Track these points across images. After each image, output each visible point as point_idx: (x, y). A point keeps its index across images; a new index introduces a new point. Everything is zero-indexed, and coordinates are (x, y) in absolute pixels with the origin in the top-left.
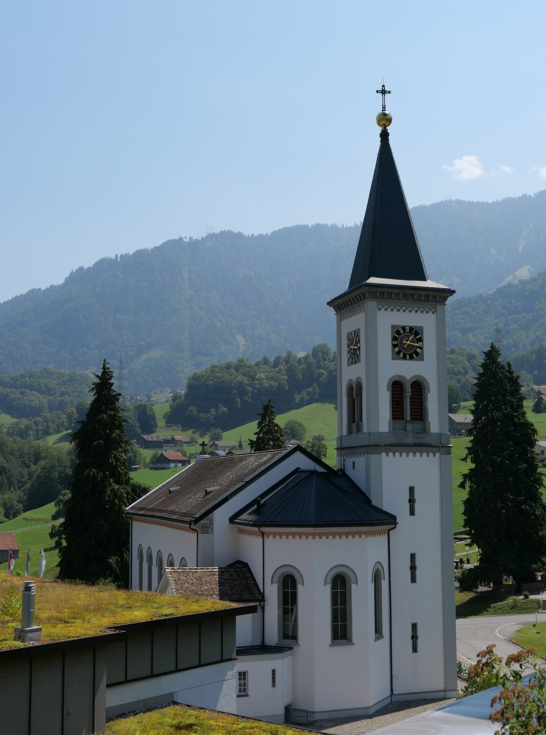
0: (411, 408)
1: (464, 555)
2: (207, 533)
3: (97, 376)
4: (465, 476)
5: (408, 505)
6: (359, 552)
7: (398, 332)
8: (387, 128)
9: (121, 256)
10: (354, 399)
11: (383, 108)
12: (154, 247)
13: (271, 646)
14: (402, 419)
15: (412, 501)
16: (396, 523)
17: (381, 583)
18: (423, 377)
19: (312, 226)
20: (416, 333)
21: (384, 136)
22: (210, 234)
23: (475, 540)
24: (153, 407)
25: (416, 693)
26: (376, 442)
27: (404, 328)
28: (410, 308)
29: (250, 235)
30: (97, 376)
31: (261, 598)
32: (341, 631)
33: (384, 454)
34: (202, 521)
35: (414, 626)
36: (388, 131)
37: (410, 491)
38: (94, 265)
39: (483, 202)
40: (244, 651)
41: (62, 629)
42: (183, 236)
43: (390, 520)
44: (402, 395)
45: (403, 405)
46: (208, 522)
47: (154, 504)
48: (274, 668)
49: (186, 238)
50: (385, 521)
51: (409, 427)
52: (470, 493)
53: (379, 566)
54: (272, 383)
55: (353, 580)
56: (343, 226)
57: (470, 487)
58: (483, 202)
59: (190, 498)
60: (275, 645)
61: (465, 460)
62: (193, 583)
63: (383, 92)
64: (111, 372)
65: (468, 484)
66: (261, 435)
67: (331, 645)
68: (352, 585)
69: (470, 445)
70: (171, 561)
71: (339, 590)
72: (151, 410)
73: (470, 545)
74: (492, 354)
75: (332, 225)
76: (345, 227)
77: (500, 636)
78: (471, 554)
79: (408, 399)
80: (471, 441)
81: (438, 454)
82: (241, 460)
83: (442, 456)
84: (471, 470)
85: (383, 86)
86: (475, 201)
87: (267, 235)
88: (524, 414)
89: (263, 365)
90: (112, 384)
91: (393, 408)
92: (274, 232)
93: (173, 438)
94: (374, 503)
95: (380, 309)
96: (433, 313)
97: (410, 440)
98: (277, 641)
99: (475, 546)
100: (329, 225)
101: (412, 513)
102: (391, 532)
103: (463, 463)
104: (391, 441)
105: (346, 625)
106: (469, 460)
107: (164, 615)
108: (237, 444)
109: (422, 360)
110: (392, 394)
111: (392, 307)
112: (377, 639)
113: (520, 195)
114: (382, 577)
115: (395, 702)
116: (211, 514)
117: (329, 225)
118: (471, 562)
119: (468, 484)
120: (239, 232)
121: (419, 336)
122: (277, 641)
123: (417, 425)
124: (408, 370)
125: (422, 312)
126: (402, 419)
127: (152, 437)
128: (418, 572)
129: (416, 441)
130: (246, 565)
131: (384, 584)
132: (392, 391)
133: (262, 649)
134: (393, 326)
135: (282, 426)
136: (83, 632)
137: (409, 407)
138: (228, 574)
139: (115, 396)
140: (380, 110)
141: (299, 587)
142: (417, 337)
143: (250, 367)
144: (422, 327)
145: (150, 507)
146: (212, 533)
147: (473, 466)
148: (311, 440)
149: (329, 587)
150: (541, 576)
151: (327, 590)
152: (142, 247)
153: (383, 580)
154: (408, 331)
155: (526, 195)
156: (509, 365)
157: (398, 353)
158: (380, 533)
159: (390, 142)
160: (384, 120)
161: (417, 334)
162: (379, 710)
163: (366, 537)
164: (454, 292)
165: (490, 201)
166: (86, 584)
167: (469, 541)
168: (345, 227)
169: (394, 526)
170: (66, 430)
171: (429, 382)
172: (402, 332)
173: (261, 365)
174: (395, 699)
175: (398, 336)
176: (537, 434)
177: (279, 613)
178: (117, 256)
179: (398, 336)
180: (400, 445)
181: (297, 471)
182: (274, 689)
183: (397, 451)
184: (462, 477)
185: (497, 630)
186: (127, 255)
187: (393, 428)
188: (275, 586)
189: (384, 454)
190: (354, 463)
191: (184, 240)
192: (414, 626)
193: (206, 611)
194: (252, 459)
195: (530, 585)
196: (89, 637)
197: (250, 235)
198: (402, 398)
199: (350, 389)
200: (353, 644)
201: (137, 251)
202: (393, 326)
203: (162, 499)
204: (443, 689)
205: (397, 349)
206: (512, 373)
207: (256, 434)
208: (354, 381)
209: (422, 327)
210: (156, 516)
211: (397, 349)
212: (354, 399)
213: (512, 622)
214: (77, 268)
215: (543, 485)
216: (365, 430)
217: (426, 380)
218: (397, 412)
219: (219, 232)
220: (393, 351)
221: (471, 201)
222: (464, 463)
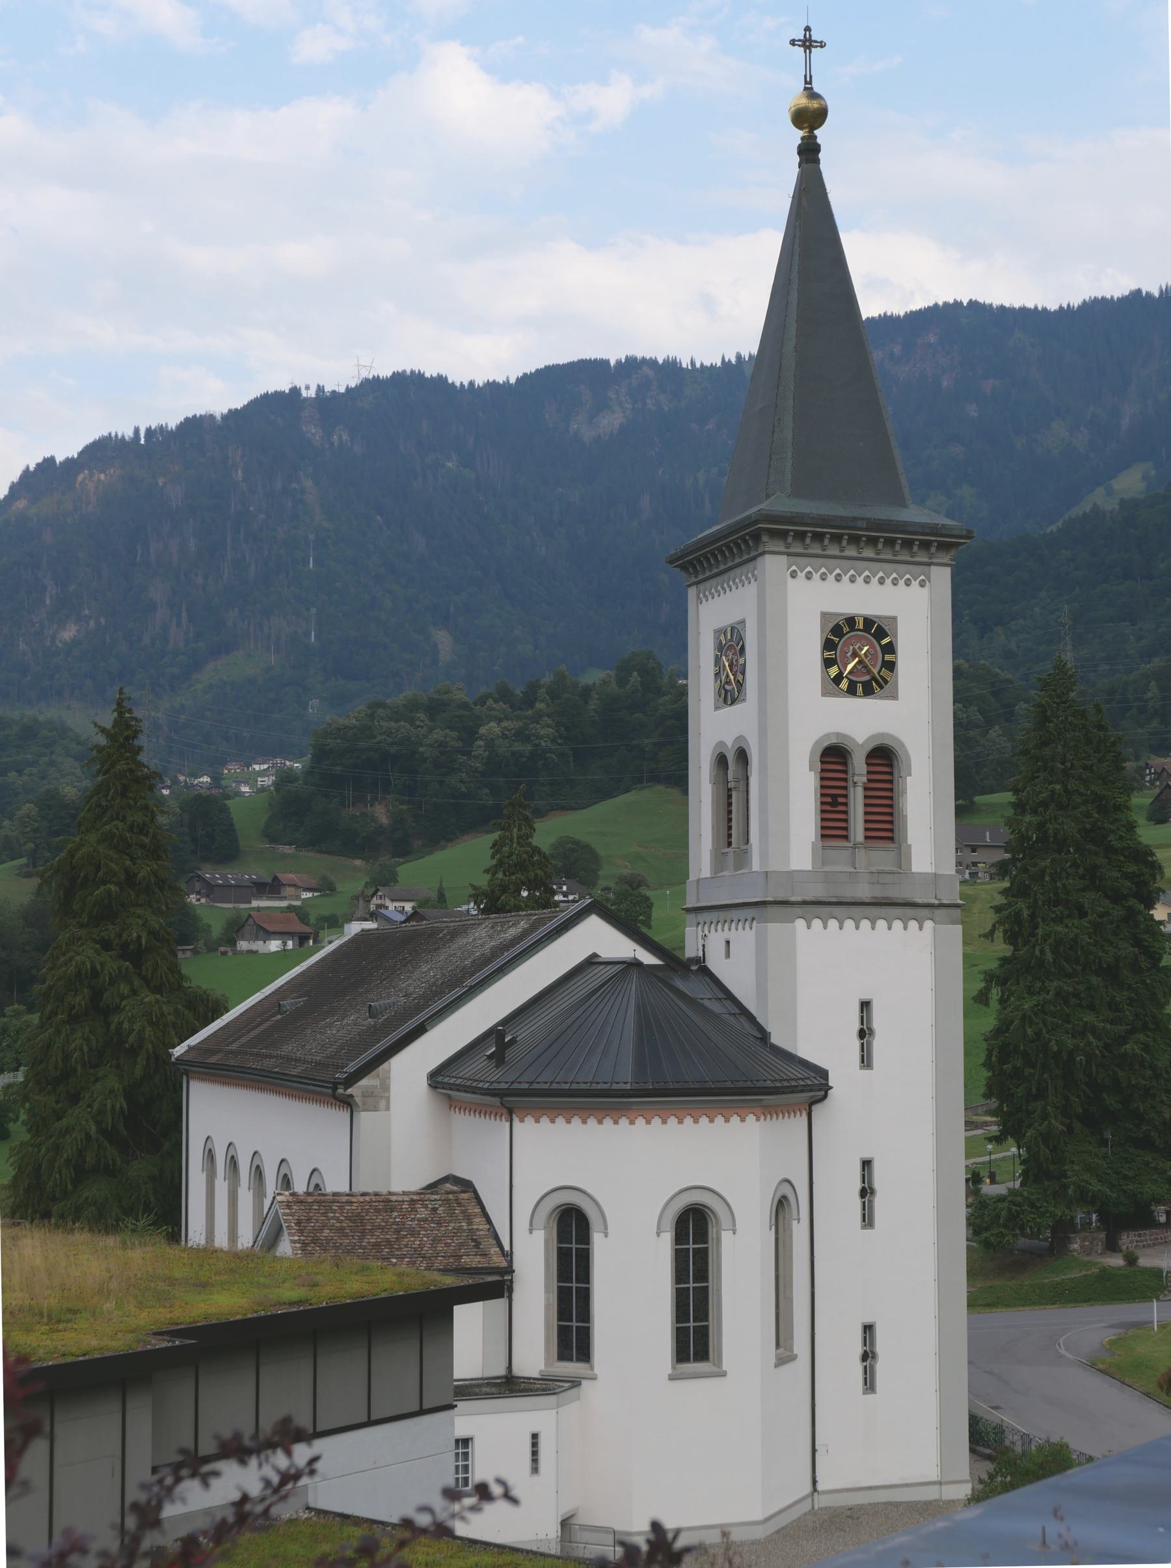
1: (983, 1163)
2: (376, 1109)
3: (103, 730)
4: (989, 977)
6: (726, 1155)
9: (149, 431)
11: (806, 83)
12: (230, 411)
13: (529, 1378)
16: (826, 1088)
19: (619, 362)
20: (878, 631)
21: (809, 152)
22: (367, 380)
24: (228, 802)
25: (870, 1488)
26: (781, 896)
29: (466, 384)
30: (103, 730)
31: (504, 1264)
32: (694, 1340)
34: (364, 1082)
35: (868, 1329)
36: (819, 141)
38: (81, 454)
39: (1036, 308)
40: (471, 1391)
41: (44, 1337)
42: (300, 384)
46: (377, 1082)
47: (244, 1040)
48: (535, 1430)
49: (307, 388)
51: (861, 854)
54: (518, 747)
56: (693, 363)
58: (1036, 308)
59: (330, 1026)
60: (537, 1375)
62: (342, 1229)
63: (807, 43)
64: (136, 719)
65: (995, 993)
66: (500, 875)
67: (672, 1378)
68: (723, 1233)
69: (1000, 900)
70: (285, 1175)
72: (224, 810)
73: (998, 1140)
75: (666, 362)
76: (698, 365)
77: (1069, 1356)
80: (1005, 892)
82: (454, 934)
85: (808, 29)
86: (1017, 305)
87: (507, 384)
88: (1131, 827)
89: (496, 701)
90: (140, 749)
92: (525, 375)
93: (275, 879)
94: (775, 1039)
95: (794, 575)
97: (864, 891)
98: (543, 1368)
99: (1010, 1140)
100: (660, 361)
101: (866, 1061)
102: (814, 1108)
106: (999, 934)
107: (285, 1303)
108: (434, 895)
112: (781, 1362)
114: (795, 1216)
115: (820, 1509)
116: (385, 1065)
117: (660, 361)
118: (997, 1178)
120: (440, 377)
122: (543, 1368)
123: (881, 857)
124: (860, 721)
127: (224, 877)
129: (878, 893)
130: (467, 1185)
131: (799, 1231)
132: (823, 770)
133: (509, 1385)
135: (545, 848)
136: (94, 1343)
137: (860, 810)
138: (426, 1207)
139: (147, 777)
141: (597, 1238)
143: (465, 706)
144: (895, 619)
145: (234, 1047)
146: (388, 1108)
148: (612, 885)
149: (668, 1238)
150: (1167, 1213)
151: (664, 1248)
152: (200, 411)
153: (795, 1223)
154: (861, 627)
155: (1139, 291)
157: (838, 679)
159: (823, 166)
160: (810, 118)
161: (881, 633)
162: (783, 1528)
165: (1053, 307)
166: (91, 1230)
167: (994, 1129)
168: (698, 365)
170: (13, 859)
173: (490, 702)
174: (821, 1502)
176: (1162, 873)
177: (547, 1299)
178: (137, 431)
181: (592, 961)
182: (535, 1478)
184: (982, 977)
186: (162, 429)
187: (820, 857)
188: (540, 1236)
189: (800, 924)
190: (728, 942)
191: (304, 393)
192: (868, 1329)
193: (384, 1295)
194: (481, 932)
195: (1140, 1236)
196: (110, 1354)
197: (466, 384)
199: (721, 761)
200: (724, 1374)
201: (187, 419)
203: (263, 1027)
204: (935, 1478)
205: (833, 671)
207: (487, 871)
208: (730, 745)
209: (895, 619)
210: (235, 1067)
211: (833, 671)
214: (40, 460)
216: (756, 866)
217: (902, 745)
218: (832, 824)
219: (389, 374)
221: (1007, 305)
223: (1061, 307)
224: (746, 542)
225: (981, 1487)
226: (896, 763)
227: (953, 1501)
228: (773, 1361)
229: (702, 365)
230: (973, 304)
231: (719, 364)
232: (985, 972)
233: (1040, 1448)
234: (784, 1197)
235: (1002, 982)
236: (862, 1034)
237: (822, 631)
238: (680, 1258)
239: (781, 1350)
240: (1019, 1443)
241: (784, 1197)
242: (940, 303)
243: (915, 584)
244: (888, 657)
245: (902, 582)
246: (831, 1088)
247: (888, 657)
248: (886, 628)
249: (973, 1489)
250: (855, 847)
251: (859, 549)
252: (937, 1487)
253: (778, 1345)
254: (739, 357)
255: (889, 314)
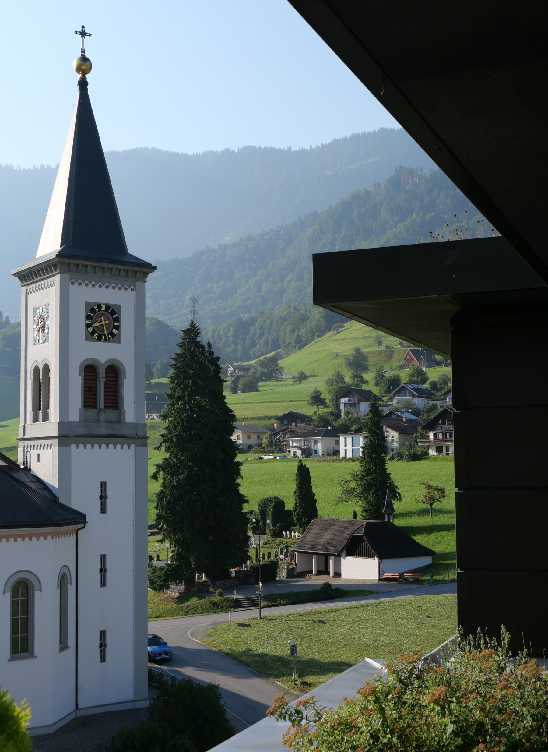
0: (105, 395)
4: (159, 466)
5: (99, 502)
7: (92, 311)
8: (86, 76)
10: (40, 384)
11: (82, 52)
14: (95, 407)
15: (103, 497)
17: (67, 589)
18: (119, 361)
20: (112, 312)
21: (83, 85)
23: (169, 535)
27: (99, 306)
28: (107, 284)
33: (73, 446)
36: (87, 80)
37: (102, 487)
39: (182, 153)
43: (78, 519)
44: (96, 380)
45: (96, 391)
50: (73, 521)
52: (164, 485)
53: (65, 570)
55: (36, 586)
57: (165, 478)
58: (182, 153)
61: (158, 448)
63: (83, 34)
67: (9, 660)
71: (20, 599)
73: (161, 541)
74: (192, 332)
76: (22, 169)
78: (163, 551)
79: (102, 385)
81: (133, 446)
83: (139, 448)
84: (166, 459)
86: (174, 151)
91: (85, 395)
94: (61, 501)
95: (73, 283)
96: (132, 290)
97: (103, 431)
101: (103, 510)
102: (79, 532)
103: (157, 452)
104: (82, 431)
105: (28, 636)
106: (163, 449)
109: (119, 342)
110: (84, 379)
111: (87, 282)
113: (223, 150)
114: (69, 582)
115: (79, 717)
119: (161, 474)
121: (116, 315)
123: (111, 414)
124: (102, 353)
125: (120, 288)
126: (95, 407)
128: (108, 574)
129: (110, 432)
131: (71, 589)
134: (87, 304)
137: (102, 394)
140: (79, 55)
142: (114, 317)
144: (120, 306)
147: (167, 455)
149: (8, 595)
153: (69, 585)
154: (104, 309)
156: (209, 345)
157: (93, 333)
158: (68, 533)
160: (84, 65)
161: (113, 312)
162: (62, 727)
163: (53, 538)
164: (155, 268)
165: (190, 153)
167: (160, 537)
168: (22, 169)
169: (83, 525)
171: (126, 367)
172: (97, 310)
174: (80, 713)
175: (92, 315)
179: (92, 315)
180: (92, 436)
183: (88, 443)
184: (155, 467)
185: (189, 633)
189: (73, 446)
190: (39, 455)
195: (223, 583)
198: (96, 384)
202: (87, 304)
204: (132, 699)
205: (91, 329)
206: (212, 353)
209: (120, 306)
211: (91, 329)
212: (40, 384)
213: (205, 623)
215: (240, 475)
217: (122, 364)
220: (87, 331)
222: (158, 451)
223: (194, 154)
224: (50, 268)
225: (153, 702)
226: (119, 372)
227: (141, 709)
228: (58, 649)
229: (24, 169)
230: (153, 149)
231: (32, 169)
232: (157, 465)
233: (180, 683)
234: (65, 574)
235: (163, 470)
236: (101, 497)
237: (86, 310)
238: (14, 605)
239: (62, 645)
240: (170, 681)
241: (65, 574)
242: (138, 148)
243: (129, 290)
244: (116, 324)
245: (123, 289)
246: (87, 522)
247: (116, 324)
248: (115, 310)
249: (150, 704)
250: (99, 411)
251: (229, 589)
252: (133, 703)
253: (61, 643)
254: (42, 166)
255: (114, 151)
